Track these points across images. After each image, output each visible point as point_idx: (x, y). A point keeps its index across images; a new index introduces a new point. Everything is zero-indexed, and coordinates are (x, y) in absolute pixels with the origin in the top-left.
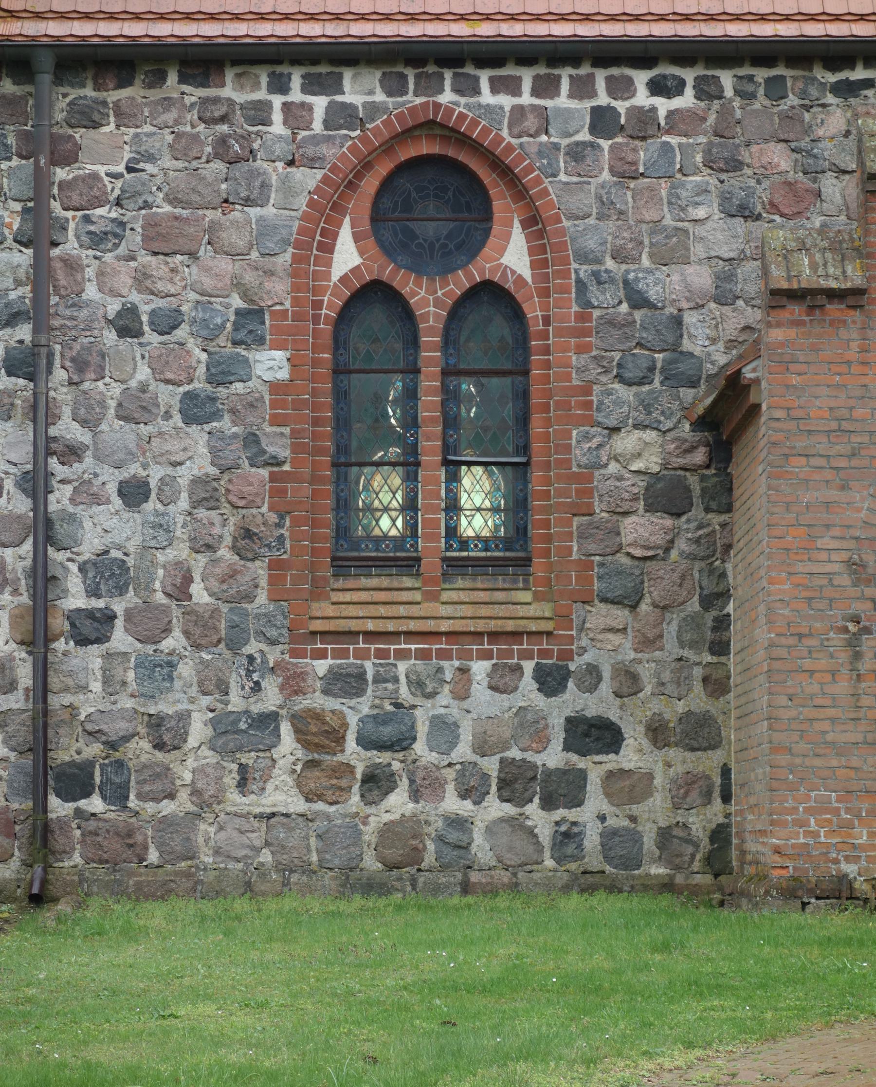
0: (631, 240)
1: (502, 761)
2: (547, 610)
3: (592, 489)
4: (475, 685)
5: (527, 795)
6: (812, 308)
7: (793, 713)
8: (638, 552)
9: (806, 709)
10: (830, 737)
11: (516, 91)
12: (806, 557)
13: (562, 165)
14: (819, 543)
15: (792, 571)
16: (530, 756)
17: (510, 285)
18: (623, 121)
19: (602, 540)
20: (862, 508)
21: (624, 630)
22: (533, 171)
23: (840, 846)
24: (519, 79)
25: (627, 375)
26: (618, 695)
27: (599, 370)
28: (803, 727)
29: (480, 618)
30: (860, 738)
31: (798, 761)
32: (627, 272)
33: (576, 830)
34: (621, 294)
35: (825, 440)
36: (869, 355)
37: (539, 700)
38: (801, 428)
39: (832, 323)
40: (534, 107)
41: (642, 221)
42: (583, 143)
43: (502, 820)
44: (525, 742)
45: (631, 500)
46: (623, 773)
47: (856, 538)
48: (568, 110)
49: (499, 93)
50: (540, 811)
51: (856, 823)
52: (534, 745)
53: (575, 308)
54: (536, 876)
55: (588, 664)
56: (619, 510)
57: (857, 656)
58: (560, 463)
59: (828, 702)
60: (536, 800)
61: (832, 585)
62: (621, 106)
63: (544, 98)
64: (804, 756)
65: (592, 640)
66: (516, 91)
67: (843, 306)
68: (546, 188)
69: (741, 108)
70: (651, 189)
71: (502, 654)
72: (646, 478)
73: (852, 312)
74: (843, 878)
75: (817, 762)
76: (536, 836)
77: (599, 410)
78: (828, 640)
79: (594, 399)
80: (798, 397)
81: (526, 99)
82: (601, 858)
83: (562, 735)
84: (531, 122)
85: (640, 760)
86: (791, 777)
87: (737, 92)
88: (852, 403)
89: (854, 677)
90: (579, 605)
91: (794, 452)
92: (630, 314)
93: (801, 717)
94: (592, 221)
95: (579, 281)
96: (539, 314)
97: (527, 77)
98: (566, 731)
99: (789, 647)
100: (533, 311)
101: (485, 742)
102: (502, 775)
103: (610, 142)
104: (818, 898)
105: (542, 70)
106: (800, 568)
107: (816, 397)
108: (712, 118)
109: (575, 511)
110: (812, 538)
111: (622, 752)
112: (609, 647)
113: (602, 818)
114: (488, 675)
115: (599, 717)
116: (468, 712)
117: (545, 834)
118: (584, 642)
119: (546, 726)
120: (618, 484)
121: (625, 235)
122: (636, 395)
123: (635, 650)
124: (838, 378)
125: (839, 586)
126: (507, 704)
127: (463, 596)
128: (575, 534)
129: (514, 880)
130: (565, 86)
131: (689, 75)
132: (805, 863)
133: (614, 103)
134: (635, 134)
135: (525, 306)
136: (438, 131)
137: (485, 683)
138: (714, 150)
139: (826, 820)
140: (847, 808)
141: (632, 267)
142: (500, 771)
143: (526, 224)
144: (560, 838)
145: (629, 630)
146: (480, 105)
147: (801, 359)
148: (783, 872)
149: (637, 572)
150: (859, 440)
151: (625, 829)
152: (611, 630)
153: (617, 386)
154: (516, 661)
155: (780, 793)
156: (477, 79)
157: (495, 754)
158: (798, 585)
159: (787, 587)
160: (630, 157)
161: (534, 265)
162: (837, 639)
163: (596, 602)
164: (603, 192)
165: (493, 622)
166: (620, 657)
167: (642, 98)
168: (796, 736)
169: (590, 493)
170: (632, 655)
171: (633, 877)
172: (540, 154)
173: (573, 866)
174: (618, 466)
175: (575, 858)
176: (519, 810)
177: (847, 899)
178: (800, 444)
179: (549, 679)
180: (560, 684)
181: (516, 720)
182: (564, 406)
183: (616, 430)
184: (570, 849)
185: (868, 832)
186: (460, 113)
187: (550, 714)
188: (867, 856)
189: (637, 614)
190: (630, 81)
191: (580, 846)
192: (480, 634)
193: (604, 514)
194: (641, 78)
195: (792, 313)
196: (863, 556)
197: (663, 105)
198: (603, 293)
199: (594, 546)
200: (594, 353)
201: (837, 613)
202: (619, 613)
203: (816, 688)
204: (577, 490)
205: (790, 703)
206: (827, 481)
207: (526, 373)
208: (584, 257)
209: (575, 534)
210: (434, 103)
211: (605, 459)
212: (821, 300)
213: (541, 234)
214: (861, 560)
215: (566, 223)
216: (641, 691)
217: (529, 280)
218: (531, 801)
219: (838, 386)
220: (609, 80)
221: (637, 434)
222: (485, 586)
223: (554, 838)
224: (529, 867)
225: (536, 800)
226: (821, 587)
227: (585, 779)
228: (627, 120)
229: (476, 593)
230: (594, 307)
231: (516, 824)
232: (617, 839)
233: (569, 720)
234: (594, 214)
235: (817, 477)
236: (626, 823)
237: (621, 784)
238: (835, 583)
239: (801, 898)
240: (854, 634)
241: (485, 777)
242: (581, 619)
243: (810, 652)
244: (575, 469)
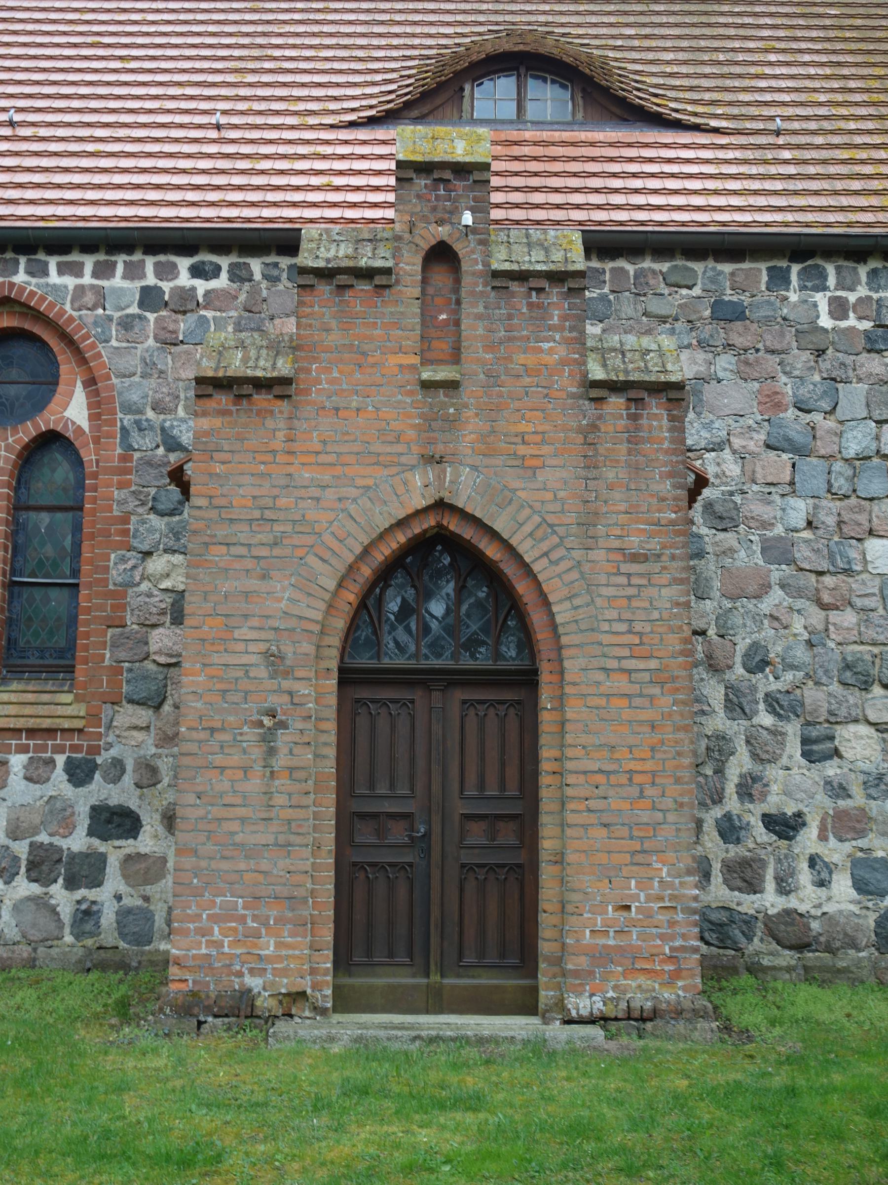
0: (169, 394)
1: (31, 844)
2: (81, 709)
3: (125, 604)
4: (12, 776)
5: (52, 875)
6: (239, 397)
7: (201, 812)
8: (162, 660)
9: (215, 808)
10: (238, 838)
11: (79, 274)
12: (222, 648)
13: (114, 333)
14: (237, 634)
15: (207, 661)
16: (57, 841)
17: (70, 434)
18: (166, 298)
19: (131, 649)
20: (283, 598)
21: (147, 728)
22: (90, 337)
23: (244, 957)
24: (82, 264)
25: (160, 507)
26: (138, 786)
27: (137, 503)
28: (211, 827)
29: (23, 716)
30: (271, 839)
31: (203, 864)
32: (164, 421)
33: (95, 908)
34: (159, 439)
35: (247, 528)
36: (295, 444)
37: (67, 790)
38: (223, 516)
39: (259, 413)
40: (93, 287)
41: (179, 379)
42: (133, 316)
43: (29, 899)
44: (53, 828)
45: (158, 614)
46: (140, 857)
47: (276, 629)
48: (121, 289)
49: (64, 274)
50: (63, 890)
51: (263, 931)
52: (61, 831)
53: (119, 451)
54: (54, 952)
55: (113, 758)
56: (147, 622)
57: (272, 752)
58: (98, 582)
59: (239, 801)
60: (61, 881)
61: (248, 677)
62: (166, 286)
63: (102, 279)
64: (211, 858)
65: (118, 736)
66: (79, 274)
67: (270, 397)
68: (99, 353)
69: (268, 289)
70: (188, 353)
71: (37, 749)
72: (173, 595)
73: (279, 403)
74: (247, 995)
75: (225, 865)
76: (58, 914)
77: (134, 537)
78: (241, 734)
79: (131, 527)
80: (221, 486)
81: (87, 279)
82: (116, 934)
83: (87, 822)
84: (89, 298)
85: (155, 845)
86: (195, 881)
87: (265, 276)
88: (276, 491)
89: (268, 774)
90: (109, 705)
91: (214, 540)
92: (166, 456)
93: (210, 817)
94: (136, 379)
95: (123, 428)
96: (94, 457)
97: (89, 262)
98: (91, 818)
99: (200, 742)
100: (89, 456)
101: (18, 827)
102: (31, 858)
103: (155, 315)
104: (216, 1016)
105: (102, 257)
106: (216, 659)
107: (239, 486)
108: (243, 297)
109: (109, 623)
110: (230, 629)
111: (140, 838)
112: (133, 743)
113: (118, 898)
114: (24, 767)
115: (120, 806)
116: (4, 800)
117: (66, 911)
118: (110, 739)
119: (73, 814)
120: (147, 600)
121: (164, 390)
122: (167, 524)
123: (156, 746)
124: (262, 467)
125: (255, 678)
126: (39, 793)
127: (13, 697)
128: (109, 643)
129: (33, 955)
130: (120, 269)
131: (225, 262)
132: (206, 975)
133: (160, 284)
134: (177, 308)
135: (82, 452)
136: (17, 309)
137: (21, 775)
138: (243, 322)
139: (230, 928)
140: (254, 915)
141: (169, 417)
142: (30, 853)
143: (87, 384)
144: (80, 915)
145: (152, 728)
146: (47, 285)
147: (225, 448)
148: (182, 986)
149: (161, 677)
150: (282, 529)
151: (138, 908)
152: (136, 728)
153: (152, 516)
154: (49, 754)
155: (183, 898)
156: (46, 264)
157: (25, 838)
158: (213, 677)
159: (201, 679)
160: (171, 327)
161: (91, 418)
162: (251, 734)
163: (124, 703)
164: (147, 355)
165: (32, 720)
166: (142, 752)
167: (184, 279)
168: (202, 837)
169: (123, 607)
170: (153, 750)
171: (143, 953)
172: (96, 324)
173: (89, 942)
174: (150, 585)
175: (92, 935)
176: (44, 890)
177: (247, 1017)
178: (221, 532)
179: (78, 771)
180: (87, 776)
181: (47, 808)
182: (107, 533)
183: (148, 554)
184: (88, 927)
185: (275, 943)
186: (31, 291)
187: (77, 802)
188: (274, 969)
189: (160, 714)
190: (174, 266)
191: (97, 925)
192: (20, 730)
193: (134, 626)
194: (184, 263)
195: (219, 403)
196: (282, 647)
197: (201, 286)
198: (144, 438)
199: (124, 654)
200: (133, 488)
201: (252, 707)
202: (144, 713)
203: (227, 785)
204: (112, 606)
205: (198, 801)
206: (248, 571)
207: (81, 509)
208: (128, 409)
209: (109, 643)
210: (10, 282)
211: (138, 578)
212: (247, 389)
213: (97, 393)
214: (279, 651)
215: (115, 380)
216: (160, 782)
217: (87, 430)
218: (55, 881)
219: (262, 475)
220: (156, 265)
221: (167, 557)
222: (35, 689)
223: (75, 915)
224: (50, 943)
225: (61, 881)
226: (237, 679)
227: (105, 862)
228: (170, 297)
229: (25, 695)
230: (135, 450)
231: (42, 903)
232: (131, 917)
233: (93, 808)
234: (139, 373)
235: (237, 566)
236: (140, 902)
237: (138, 866)
238: (251, 675)
239: (197, 1016)
240: (269, 729)
241: (16, 859)
242: (109, 717)
243: (222, 747)
244: (111, 587)
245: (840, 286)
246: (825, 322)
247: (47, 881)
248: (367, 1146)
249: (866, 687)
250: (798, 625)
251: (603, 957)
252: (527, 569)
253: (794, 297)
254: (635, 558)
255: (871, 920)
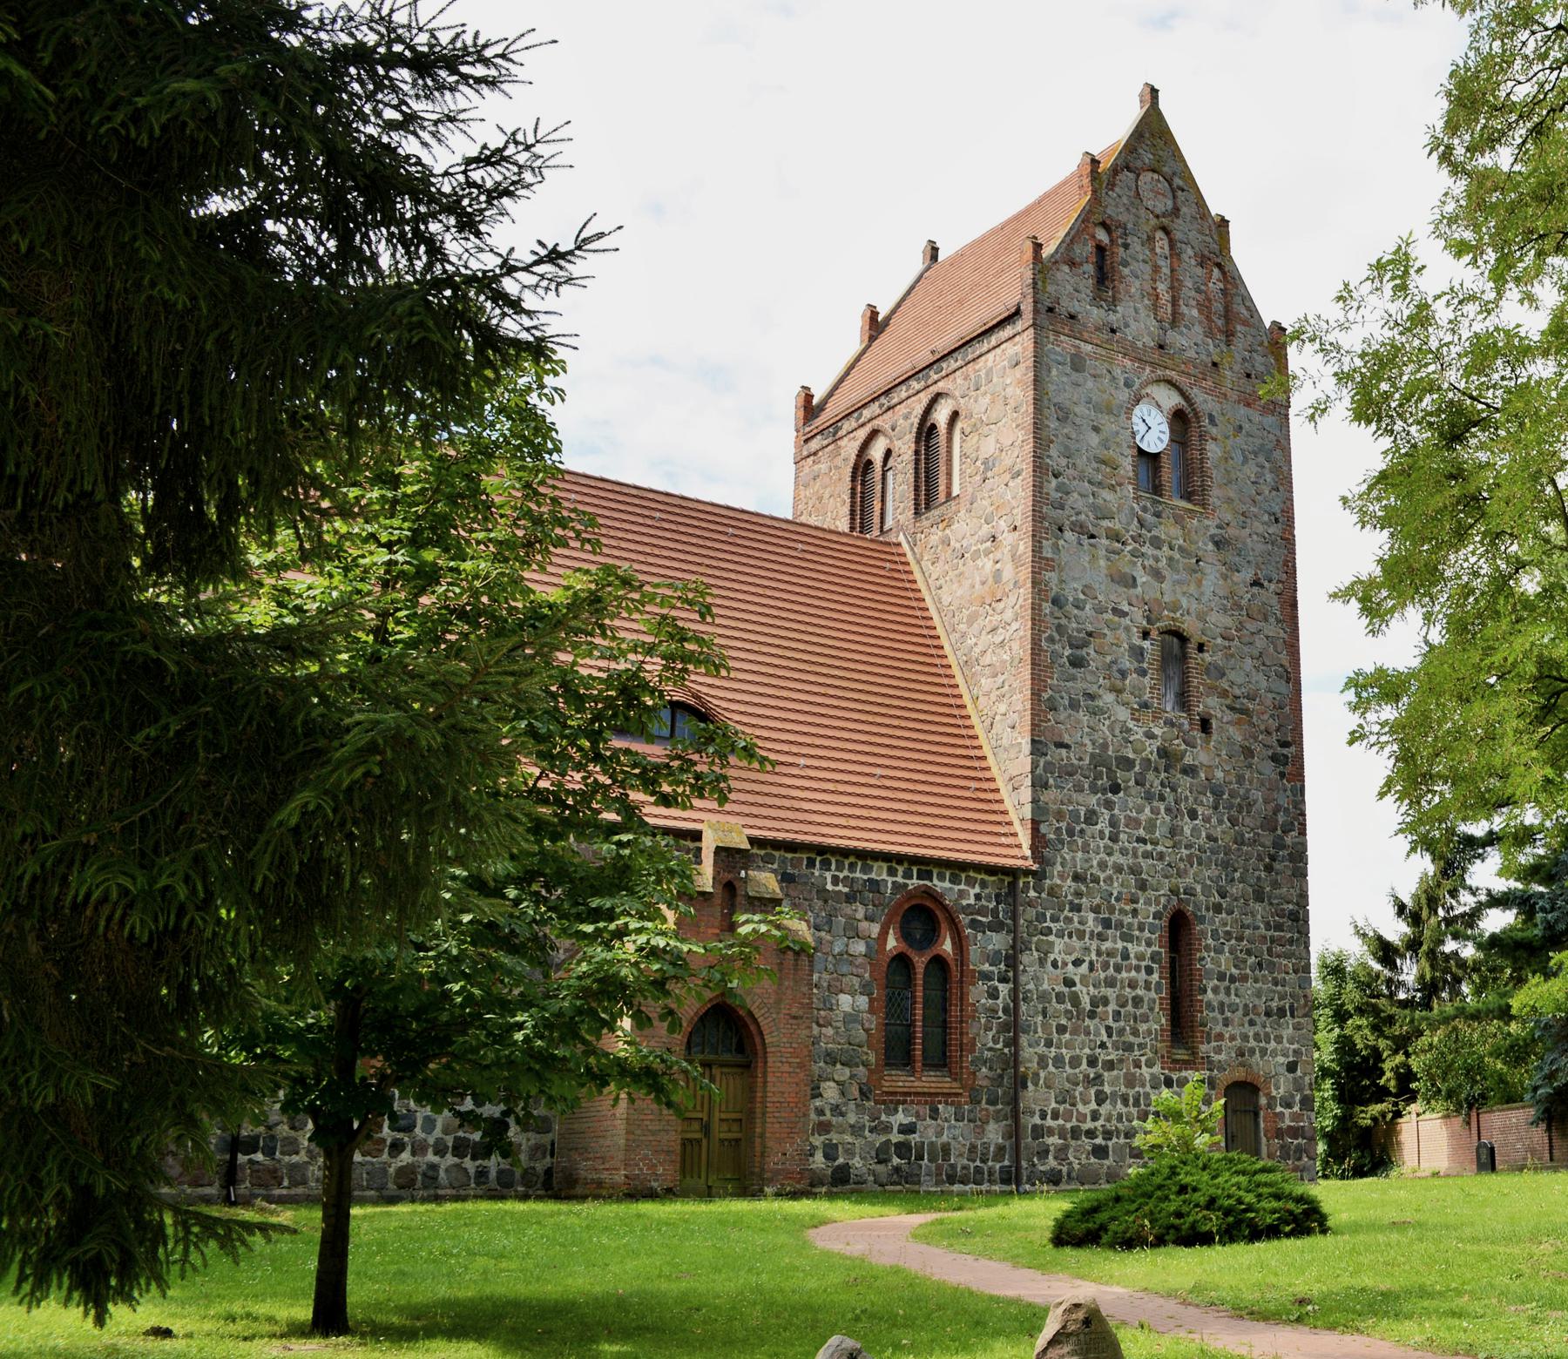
117: (472, 1171)
245: (838, 869)
246: (829, 887)
247: (462, 1156)
249: (834, 1064)
251: (778, 1172)
252: (755, 1021)
253: (817, 873)
254: (795, 1018)
255: (829, 1171)
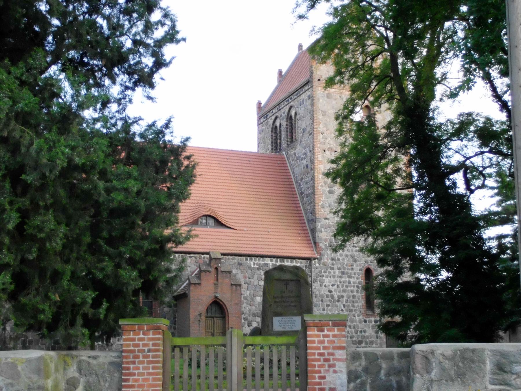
246: (252, 266)
248: (488, 46)
250: (247, 308)
253: (248, 262)
